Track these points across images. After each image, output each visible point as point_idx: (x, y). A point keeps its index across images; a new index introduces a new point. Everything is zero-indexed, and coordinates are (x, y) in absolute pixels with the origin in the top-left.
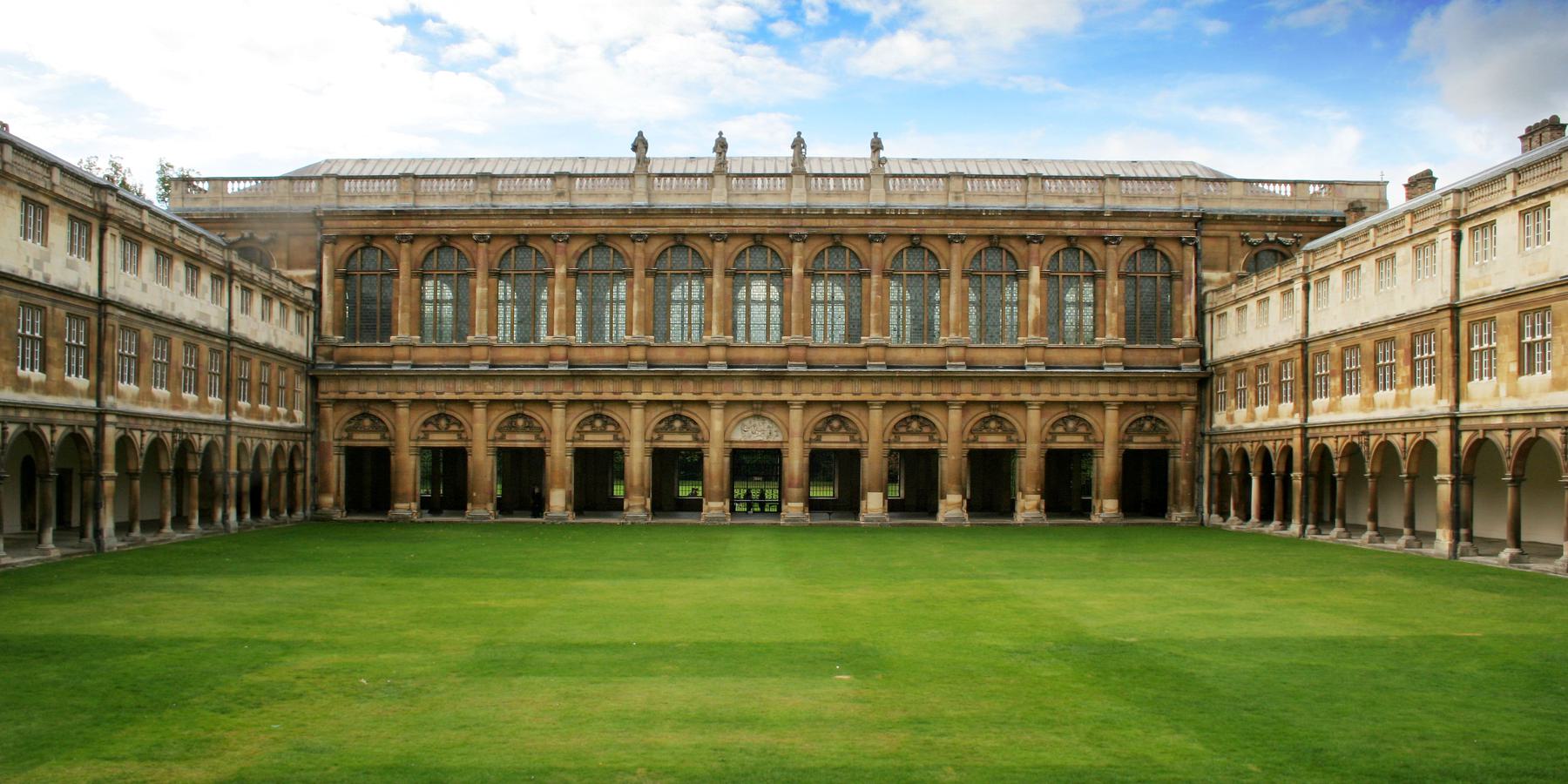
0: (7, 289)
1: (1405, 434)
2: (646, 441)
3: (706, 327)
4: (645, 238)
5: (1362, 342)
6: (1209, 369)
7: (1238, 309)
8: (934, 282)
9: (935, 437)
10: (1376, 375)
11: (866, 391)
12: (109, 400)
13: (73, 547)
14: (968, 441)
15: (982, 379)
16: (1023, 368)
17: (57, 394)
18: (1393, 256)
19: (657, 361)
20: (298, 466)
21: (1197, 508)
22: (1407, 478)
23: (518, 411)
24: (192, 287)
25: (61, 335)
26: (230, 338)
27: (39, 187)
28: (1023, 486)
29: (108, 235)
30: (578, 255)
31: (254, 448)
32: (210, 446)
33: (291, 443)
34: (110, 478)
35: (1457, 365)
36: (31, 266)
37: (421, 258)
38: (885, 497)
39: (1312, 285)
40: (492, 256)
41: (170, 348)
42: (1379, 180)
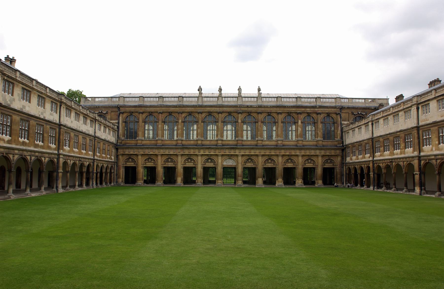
0: (33, 119)
1: (404, 162)
2: (201, 165)
3: (217, 135)
4: (201, 113)
5: (389, 138)
8: (274, 124)
10: (394, 146)
12: (61, 152)
13: (50, 191)
14: (283, 165)
15: (287, 149)
17: (46, 149)
18: (398, 114)
20: (112, 171)
22: (405, 173)
23: (169, 157)
24: (85, 123)
25: (48, 133)
26: (95, 137)
27: (43, 93)
28: (298, 177)
29: (62, 107)
30: (184, 117)
31: (101, 166)
32: (89, 165)
33: (111, 165)
34: (61, 172)
35: (419, 142)
36: (40, 114)
38: (262, 179)
39: (374, 123)
40: (163, 117)
41: (78, 138)
42: (386, 98)
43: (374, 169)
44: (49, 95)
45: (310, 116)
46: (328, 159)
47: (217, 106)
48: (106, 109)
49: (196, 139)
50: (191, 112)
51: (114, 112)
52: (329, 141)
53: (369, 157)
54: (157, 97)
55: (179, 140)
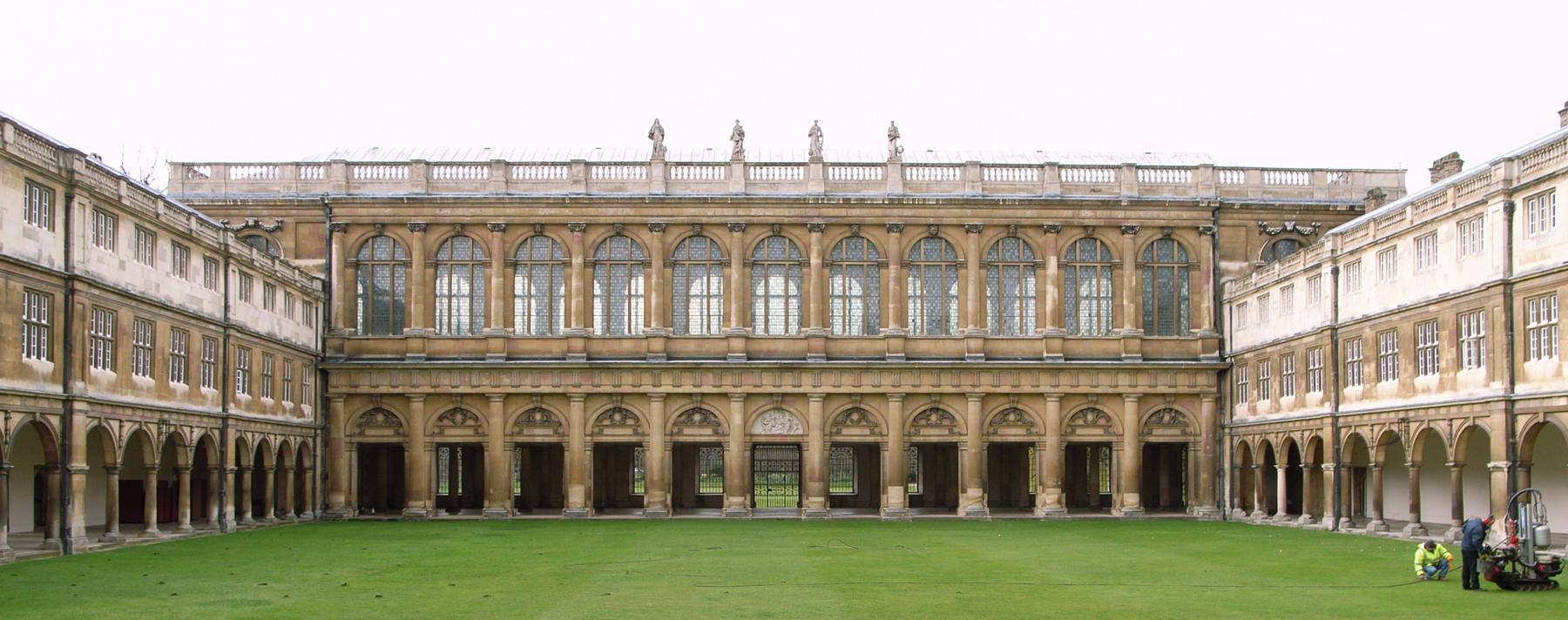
3: (726, 318)
5: (1399, 326)
6: (1228, 360)
7: (1259, 298)
8: (951, 273)
9: (955, 430)
10: (1416, 359)
11: (886, 383)
14: (988, 434)
16: (1042, 359)
17: (12, 377)
18: (1434, 234)
19: (675, 353)
20: (307, 463)
21: (1219, 502)
22: (1455, 466)
23: (536, 405)
24: (182, 269)
26: (227, 326)
29: (75, 204)
30: (596, 244)
31: (256, 443)
32: (203, 442)
33: (298, 439)
34: (80, 471)
35: (1511, 344)
37: (435, 248)
38: (906, 491)
39: (1341, 269)
41: (154, 333)
43: (1338, 450)
44: (16, 153)
45: (1096, 239)
46: (1164, 410)
47: (727, 199)
48: (275, 212)
49: (644, 332)
50: (624, 224)
51: (310, 225)
52: (1168, 338)
53: (1322, 403)
54: (483, 164)
55: (576, 337)
